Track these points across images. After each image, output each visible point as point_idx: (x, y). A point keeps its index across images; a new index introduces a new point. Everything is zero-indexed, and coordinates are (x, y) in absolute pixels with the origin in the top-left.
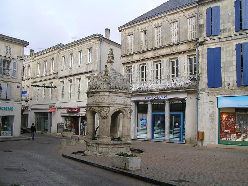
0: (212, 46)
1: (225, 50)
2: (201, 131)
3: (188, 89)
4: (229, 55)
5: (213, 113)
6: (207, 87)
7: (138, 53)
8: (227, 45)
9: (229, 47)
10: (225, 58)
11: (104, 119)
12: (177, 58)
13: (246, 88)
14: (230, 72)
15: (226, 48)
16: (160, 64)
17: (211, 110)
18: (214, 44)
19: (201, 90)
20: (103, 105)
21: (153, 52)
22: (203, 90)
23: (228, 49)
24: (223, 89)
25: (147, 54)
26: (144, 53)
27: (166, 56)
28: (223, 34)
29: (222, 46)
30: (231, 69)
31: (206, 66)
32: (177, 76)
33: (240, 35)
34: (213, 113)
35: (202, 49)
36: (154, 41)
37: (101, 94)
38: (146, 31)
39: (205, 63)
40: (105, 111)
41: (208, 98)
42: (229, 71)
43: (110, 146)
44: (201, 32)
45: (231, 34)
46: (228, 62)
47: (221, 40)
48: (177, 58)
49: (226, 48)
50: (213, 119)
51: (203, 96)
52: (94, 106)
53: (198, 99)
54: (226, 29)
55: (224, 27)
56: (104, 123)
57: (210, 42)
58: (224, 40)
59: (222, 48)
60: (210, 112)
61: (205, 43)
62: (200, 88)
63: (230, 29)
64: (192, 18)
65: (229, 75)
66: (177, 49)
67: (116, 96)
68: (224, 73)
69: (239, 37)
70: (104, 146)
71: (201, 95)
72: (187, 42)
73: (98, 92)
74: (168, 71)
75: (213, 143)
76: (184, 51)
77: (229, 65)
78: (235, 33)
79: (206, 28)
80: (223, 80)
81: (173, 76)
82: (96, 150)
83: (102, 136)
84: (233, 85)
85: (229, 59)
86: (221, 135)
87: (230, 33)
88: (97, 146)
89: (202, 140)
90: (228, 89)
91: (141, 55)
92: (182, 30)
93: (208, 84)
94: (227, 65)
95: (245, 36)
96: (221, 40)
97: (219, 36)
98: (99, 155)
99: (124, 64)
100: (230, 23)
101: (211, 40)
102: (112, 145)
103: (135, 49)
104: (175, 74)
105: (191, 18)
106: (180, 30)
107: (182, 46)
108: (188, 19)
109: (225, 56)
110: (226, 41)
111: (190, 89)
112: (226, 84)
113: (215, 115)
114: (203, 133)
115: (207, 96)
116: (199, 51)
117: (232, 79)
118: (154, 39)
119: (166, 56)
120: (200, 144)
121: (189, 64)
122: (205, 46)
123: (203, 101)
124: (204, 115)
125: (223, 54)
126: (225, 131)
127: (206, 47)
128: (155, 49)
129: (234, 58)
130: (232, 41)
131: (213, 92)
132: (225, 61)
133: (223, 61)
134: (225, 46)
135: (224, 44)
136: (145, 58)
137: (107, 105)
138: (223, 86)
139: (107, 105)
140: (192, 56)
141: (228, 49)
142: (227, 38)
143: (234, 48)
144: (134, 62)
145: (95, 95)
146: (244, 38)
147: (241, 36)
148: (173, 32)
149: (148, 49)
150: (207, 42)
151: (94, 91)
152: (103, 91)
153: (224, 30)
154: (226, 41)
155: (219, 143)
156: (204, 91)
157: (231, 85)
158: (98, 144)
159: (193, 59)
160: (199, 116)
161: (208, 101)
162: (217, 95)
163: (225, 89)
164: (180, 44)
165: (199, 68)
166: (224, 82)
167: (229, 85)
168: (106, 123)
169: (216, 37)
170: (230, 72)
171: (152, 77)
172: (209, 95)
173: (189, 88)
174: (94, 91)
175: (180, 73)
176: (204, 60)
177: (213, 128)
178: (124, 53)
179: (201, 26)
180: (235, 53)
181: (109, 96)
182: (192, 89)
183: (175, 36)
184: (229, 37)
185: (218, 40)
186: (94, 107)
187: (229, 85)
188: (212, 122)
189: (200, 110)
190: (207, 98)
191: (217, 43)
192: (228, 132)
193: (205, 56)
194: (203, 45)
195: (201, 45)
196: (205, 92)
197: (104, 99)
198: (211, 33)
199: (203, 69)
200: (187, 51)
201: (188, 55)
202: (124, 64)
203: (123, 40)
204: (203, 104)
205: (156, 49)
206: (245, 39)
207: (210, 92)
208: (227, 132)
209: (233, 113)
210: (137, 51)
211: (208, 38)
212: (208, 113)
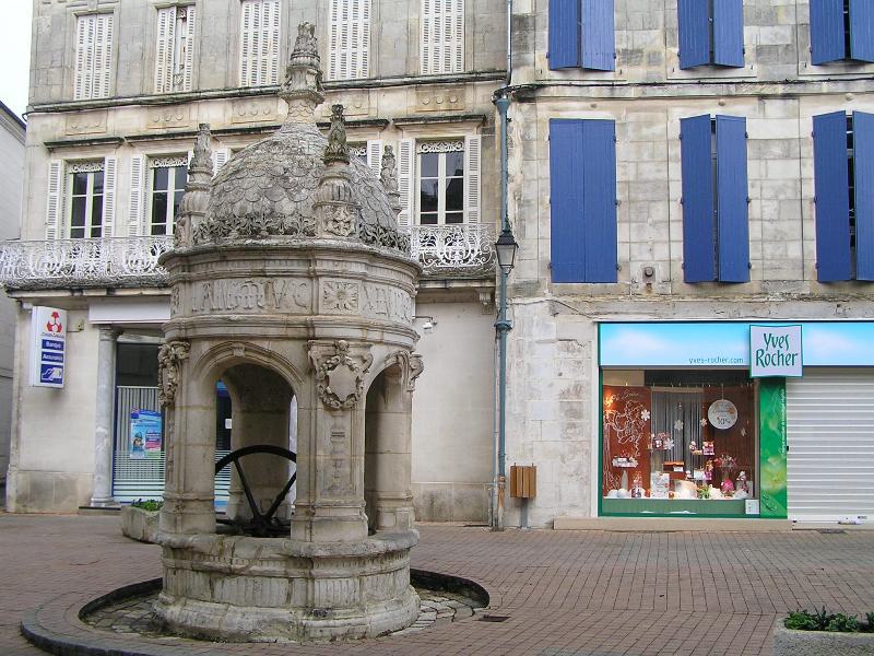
0: (574, 110)
1: (631, 135)
2: (521, 463)
3: (436, 281)
4: (652, 156)
5: (576, 387)
6: (548, 278)
7: (140, 103)
8: (643, 114)
9: (650, 124)
10: (632, 169)
11: (339, 412)
12: (102, 160)
13: (723, 290)
14: (654, 224)
15: (638, 125)
16: (99, 175)
17: (567, 374)
18: (588, 104)
19: (518, 289)
20: (338, 332)
21: (229, 106)
22: (523, 289)
23: (645, 132)
24: (625, 289)
25: (179, 112)
26: (178, 104)
27: (401, 124)
28: (625, 69)
29: (620, 119)
30: (659, 211)
31: (543, 190)
32: (96, 233)
33: (699, 83)
34: (578, 389)
35: (526, 119)
36: (236, 55)
37: (323, 266)
38: (189, 10)
39: (539, 178)
40: (351, 368)
41: (554, 323)
42: (650, 220)
43: (370, 567)
44: (522, 46)
45: (658, 73)
46: (646, 182)
47: (618, 92)
48: (102, 160)
49: (638, 125)
50: (575, 413)
51: (530, 317)
52: (272, 331)
53: (502, 329)
54: (640, 51)
55: (630, 44)
56: (341, 435)
57: (568, 92)
58: (633, 92)
59: (623, 125)
60: (563, 385)
61: (540, 93)
62: (512, 280)
63: (655, 53)
64: (94, 18)
65: (650, 234)
66: (365, 106)
67: (390, 283)
68: (626, 225)
69: (696, 91)
70: (342, 571)
71: (517, 310)
72: (416, 84)
73: (308, 254)
74: (58, 212)
75: (576, 514)
76: (403, 120)
77: (649, 196)
78: (679, 74)
79: (546, 33)
80: (622, 253)
81: (77, 234)
82: (289, 596)
83: (332, 513)
84: (666, 277)
85: (650, 171)
86: (609, 476)
87: (654, 69)
88: (294, 572)
89: (524, 503)
90: (645, 294)
91: (159, 114)
92: (393, 31)
93: (551, 266)
94: (641, 197)
95: (723, 90)
96: (618, 92)
97: (609, 76)
98: (322, 623)
99: (53, 147)
100: (657, 34)
101: (570, 85)
102: (374, 558)
103: (120, 83)
104: (88, 226)
105: (89, 18)
106: (381, 30)
107: (388, 95)
108: (77, 16)
109: (633, 157)
110: (640, 98)
111: (445, 281)
112: (636, 271)
113: (583, 395)
114: (532, 471)
115: (548, 316)
116: (511, 124)
117: (661, 252)
118: (236, 48)
119: (137, 140)
120: (514, 519)
121: (70, 196)
122: (540, 105)
123: (530, 335)
124: (532, 396)
125: (622, 150)
126: (615, 463)
127: (543, 111)
128: (242, 95)
129: (676, 171)
130: (667, 102)
131: (578, 299)
132: (631, 179)
133: (624, 178)
134: (632, 117)
135: (629, 110)
136: (181, 130)
137: (357, 334)
138: (621, 278)
139: (357, 334)
140: (166, 160)
141: (645, 132)
142: (648, 88)
143: (675, 131)
144: (117, 142)
145: (271, 267)
146: (718, 97)
147: (706, 91)
148: (432, 23)
149: (202, 88)
150: (553, 91)
151: (264, 242)
152: (338, 251)
153: (632, 55)
154: (640, 98)
155: (601, 513)
156: (531, 295)
157: (660, 274)
158: (308, 561)
159: (172, 174)
160: (507, 400)
161: (553, 336)
162: (597, 314)
163: (633, 290)
164: (378, 85)
165: (510, 196)
166: (627, 263)
167: (648, 275)
168: (347, 434)
169: (593, 77)
170: (654, 224)
171: (55, 227)
172: (558, 310)
173: (441, 277)
174: (264, 242)
175: (111, 224)
176: (534, 164)
177: (574, 451)
178: (55, 93)
179: (521, 23)
180: (676, 150)
181: (364, 278)
182: (455, 285)
183: (442, 44)
184: (655, 84)
185: (606, 92)
186: (265, 338)
187: (648, 275)
188: (573, 426)
189: (512, 374)
190: (547, 327)
191: (599, 104)
192: (628, 465)
193: (542, 149)
194: (531, 100)
195: (522, 100)
196: (537, 299)
197: (341, 294)
198: (569, 56)
199: (528, 201)
200: (421, 119)
201: (418, 136)
202: (53, 147)
203: (45, 29)
204: (526, 348)
205: (250, 94)
206: (722, 104)
207: (561, 299)
208: (623, 465)
209: (636, 389)
210: (137, 93)
211: (556, 76)
212: (551, 385)
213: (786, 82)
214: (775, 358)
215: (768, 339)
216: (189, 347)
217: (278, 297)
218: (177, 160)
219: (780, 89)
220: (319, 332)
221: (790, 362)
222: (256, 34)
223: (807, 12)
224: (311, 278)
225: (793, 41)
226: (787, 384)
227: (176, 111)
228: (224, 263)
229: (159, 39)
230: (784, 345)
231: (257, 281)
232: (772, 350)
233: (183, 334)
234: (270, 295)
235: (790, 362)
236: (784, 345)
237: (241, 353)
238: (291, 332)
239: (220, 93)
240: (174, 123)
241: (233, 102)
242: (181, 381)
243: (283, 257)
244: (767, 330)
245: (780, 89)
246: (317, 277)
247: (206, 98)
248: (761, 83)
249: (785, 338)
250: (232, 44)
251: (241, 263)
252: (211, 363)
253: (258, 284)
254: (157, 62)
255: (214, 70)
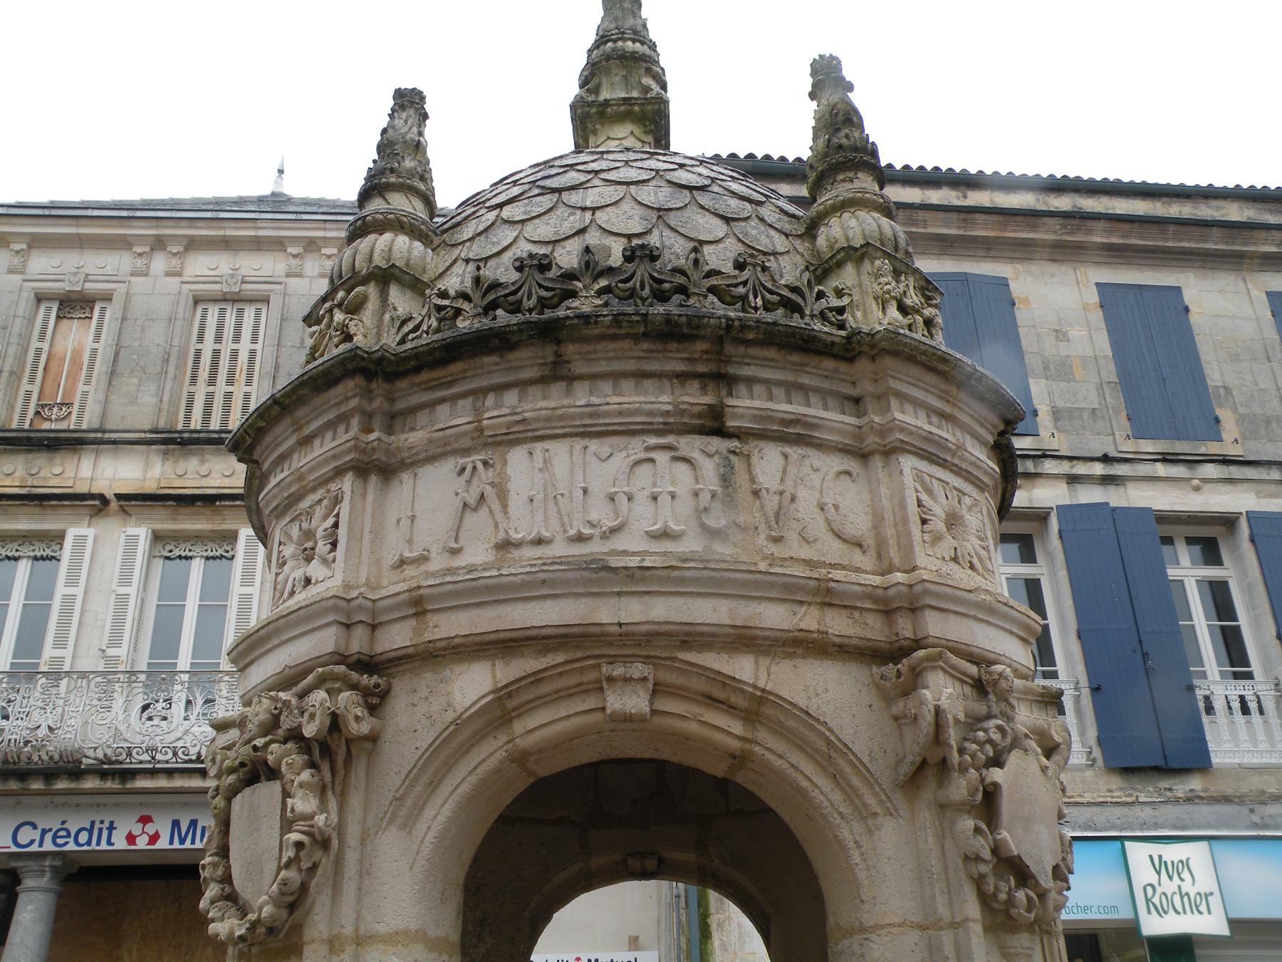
25: (58, 461)
149: (109, 426)
213: (1106, 459)
214: (1177, 899)
215: (1159, 866)
216: (385, 694)
217: (772, 502)
218: (38, 544)
219: (1098, 469)
220: (936, 626)
221: (1203, 908)
222: (216, 353)
223: (1112, 366)
224: (863, 456)
225: (1100, 404)
226: (1197, 952)
227: (52, 459)
228: (557, 388)
229: (35, 344)
230: (1186, 875)
231: (691, 445)
232: (1169, 886)
233: (358, 643)
234: (744, 495)
235: (1203, 908)
236: (1186, 875)
237: (634, 702)
238: (838, 625)
239: (143, 435)
240: (45, 479)
241: (165, 453)
242: (341, 828)
243: (778, 375)
244: (1155, 849)
245: (1098, 469)
246: (889, 452)
247: (114, 442)
248: (1071, 458)
249: (1186, 864)
250: (173, 361)
251: (627, 385)
252: (492, 753)
253: (696, 455)
254: (25, 380)
255: (134, 401)
